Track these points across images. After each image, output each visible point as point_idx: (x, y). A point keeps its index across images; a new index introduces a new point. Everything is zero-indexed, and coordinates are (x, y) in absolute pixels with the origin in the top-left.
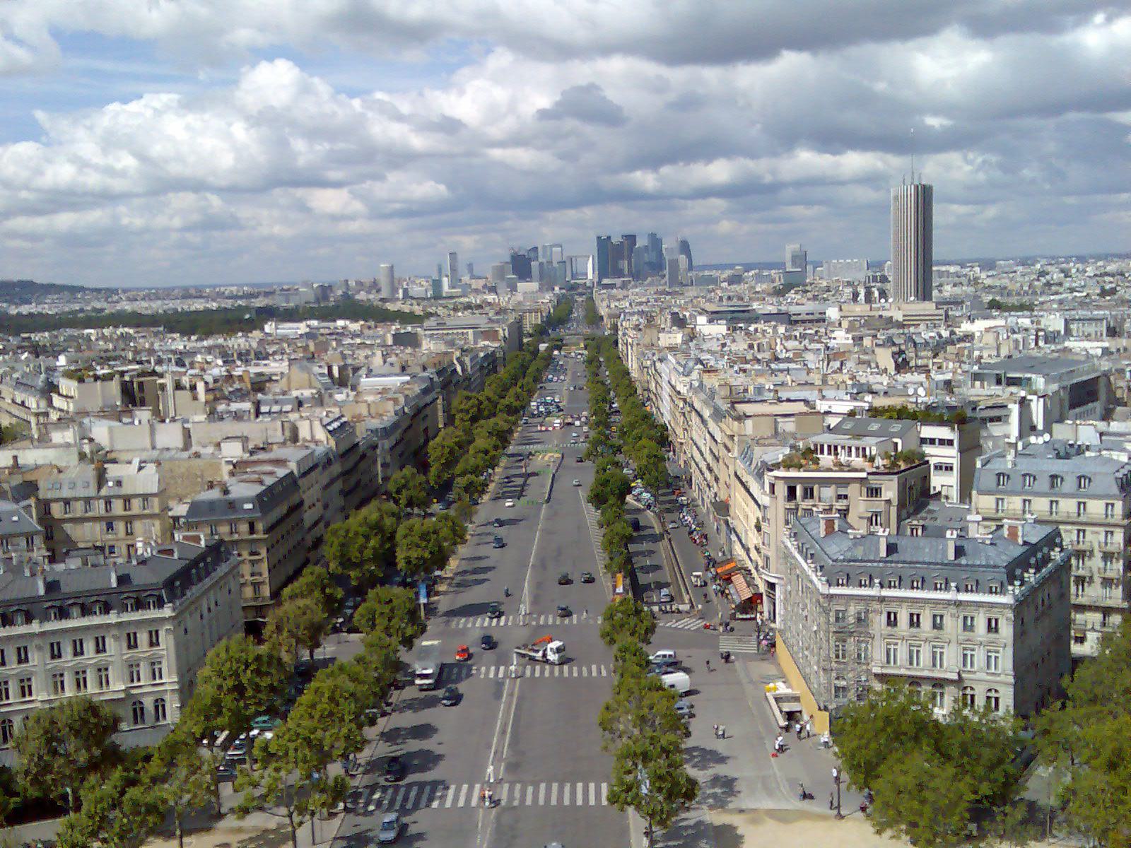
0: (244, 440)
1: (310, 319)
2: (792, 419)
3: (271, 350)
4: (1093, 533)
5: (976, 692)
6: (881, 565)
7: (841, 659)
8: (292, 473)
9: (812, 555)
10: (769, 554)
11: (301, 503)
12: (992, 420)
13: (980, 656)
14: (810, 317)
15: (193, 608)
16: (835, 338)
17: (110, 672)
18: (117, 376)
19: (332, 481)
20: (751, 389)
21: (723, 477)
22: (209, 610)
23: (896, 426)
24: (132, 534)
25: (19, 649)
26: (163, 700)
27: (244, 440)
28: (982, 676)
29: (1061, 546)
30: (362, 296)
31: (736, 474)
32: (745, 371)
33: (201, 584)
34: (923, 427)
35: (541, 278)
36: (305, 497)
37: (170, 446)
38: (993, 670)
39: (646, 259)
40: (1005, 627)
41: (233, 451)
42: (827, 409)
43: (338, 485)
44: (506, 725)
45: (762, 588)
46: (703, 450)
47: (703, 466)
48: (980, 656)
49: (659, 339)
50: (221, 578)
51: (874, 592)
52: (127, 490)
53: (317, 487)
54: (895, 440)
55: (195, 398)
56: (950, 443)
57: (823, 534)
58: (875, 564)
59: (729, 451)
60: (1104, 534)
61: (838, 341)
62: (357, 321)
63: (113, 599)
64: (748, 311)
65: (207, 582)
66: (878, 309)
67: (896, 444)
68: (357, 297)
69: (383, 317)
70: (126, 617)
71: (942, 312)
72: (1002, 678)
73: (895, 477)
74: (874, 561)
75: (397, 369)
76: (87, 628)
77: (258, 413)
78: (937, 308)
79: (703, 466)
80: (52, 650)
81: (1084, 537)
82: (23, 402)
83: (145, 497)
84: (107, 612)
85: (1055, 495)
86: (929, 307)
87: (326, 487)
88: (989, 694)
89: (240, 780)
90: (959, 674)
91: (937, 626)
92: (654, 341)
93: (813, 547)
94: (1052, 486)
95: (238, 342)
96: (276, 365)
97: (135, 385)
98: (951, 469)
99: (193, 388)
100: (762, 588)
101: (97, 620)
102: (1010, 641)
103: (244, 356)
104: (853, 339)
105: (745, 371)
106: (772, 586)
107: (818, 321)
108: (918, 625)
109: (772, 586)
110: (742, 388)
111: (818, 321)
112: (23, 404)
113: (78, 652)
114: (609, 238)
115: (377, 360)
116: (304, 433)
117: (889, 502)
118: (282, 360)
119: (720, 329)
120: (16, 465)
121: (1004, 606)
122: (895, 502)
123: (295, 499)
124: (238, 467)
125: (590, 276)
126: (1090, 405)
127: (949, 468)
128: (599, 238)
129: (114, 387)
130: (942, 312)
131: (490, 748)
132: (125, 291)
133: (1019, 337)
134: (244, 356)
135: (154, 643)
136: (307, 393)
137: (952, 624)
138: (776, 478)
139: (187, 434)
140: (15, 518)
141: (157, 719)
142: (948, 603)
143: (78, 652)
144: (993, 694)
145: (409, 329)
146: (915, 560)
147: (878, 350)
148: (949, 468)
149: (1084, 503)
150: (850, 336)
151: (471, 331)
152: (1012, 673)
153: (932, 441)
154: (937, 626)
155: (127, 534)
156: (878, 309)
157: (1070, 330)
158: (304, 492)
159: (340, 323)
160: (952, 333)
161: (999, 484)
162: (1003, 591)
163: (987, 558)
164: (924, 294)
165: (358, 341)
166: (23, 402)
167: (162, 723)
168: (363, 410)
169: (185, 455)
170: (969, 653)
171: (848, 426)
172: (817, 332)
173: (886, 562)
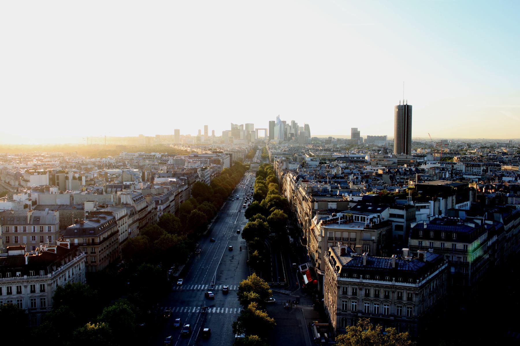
11: (118, 231)
15: (61, 275)
16: (366, 169)
19: (134, 222)
22: (69, 277)
29: (363, 330)
33: (65, 265)
36: (119, 229)
43: (137, 224)
50: (76, 263)
51: (394, 283)
53: (126, 225)
65: (69, 264)
82: (9, 182)
87: (130, 226)
89: (495, 183)
123: (115, 229)
126: (465, 203)
151: (208, 160)
158: (119, 227)
164: (408, 152)
166: (9, 182)
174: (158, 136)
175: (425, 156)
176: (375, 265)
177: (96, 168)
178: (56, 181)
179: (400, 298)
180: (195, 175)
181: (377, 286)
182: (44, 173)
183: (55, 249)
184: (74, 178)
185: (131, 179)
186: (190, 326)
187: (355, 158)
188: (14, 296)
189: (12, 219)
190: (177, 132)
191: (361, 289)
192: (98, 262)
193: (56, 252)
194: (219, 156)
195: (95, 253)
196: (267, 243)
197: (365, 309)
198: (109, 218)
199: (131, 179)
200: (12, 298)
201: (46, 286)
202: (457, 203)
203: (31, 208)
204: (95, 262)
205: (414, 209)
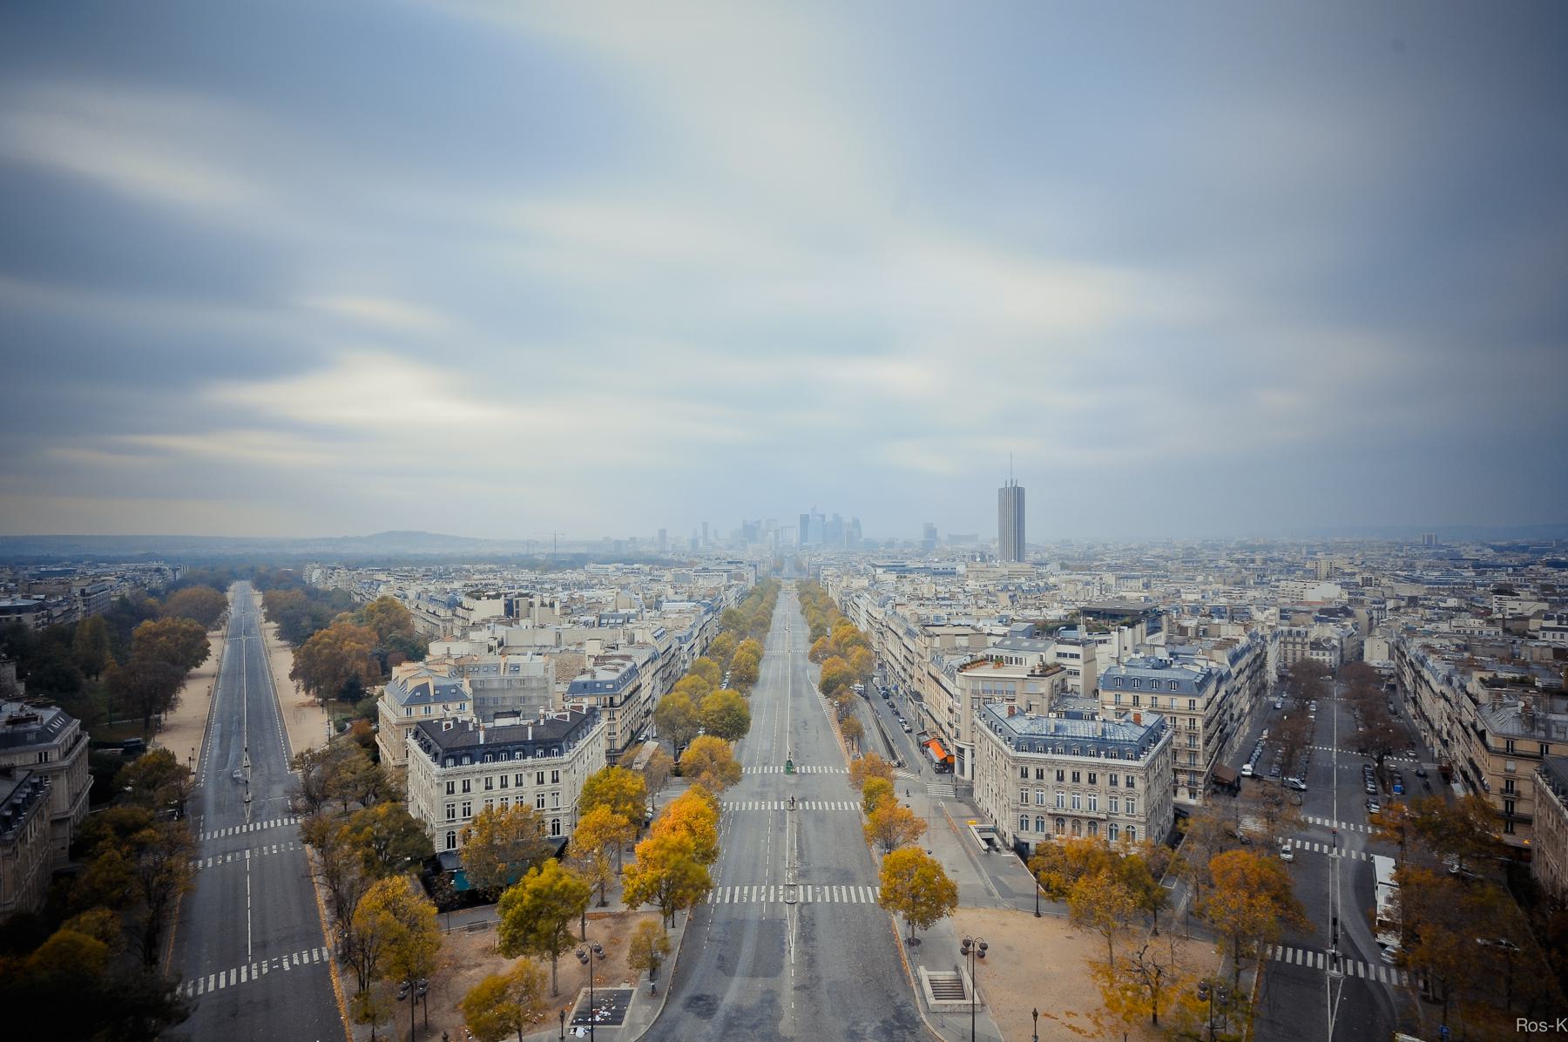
2: (967, 638)
3: (596, 581)
4: (1181, 719)
6: (1052, 738)
7: (1114, 800)
9: (1000, 730)
10: (960, 728)
12: (1100, 642)
13: (1122, 803)
18: (503, 596)
20: (932, 617)
21: (917, 674)
25: (464, 782)
26: (558, 820)
28: (1124, 817)
31: (929, 674)
32: (923, 605)
38: (1024, 803)
41: (594, 648)
43: (660, 674)
45: (954, 752)
46: (898, 657)
47: (898, 668)
48: (1122, 803)
53: (649, 675)
55: (553, 613)
56: (1077, 656)
57: (1007, 715)
58: (1047, 737)
59: (922, 658)
60: (1169, 719)
61: (970, 587)
64: (904, 566)
66: (992, 567)
69: (666, 564)
74: (1046, 735)
75: (685, 597)
77: (600, 625)
79: (898, 668)
84: (525, 758)
86: (1025, 567)
93: (1000, 724)
95: (571, 576)
97: (514, 603)
98: (1079, 674)
99: (552, 605)
100: (954, 752)
101: (519, 763)
103: (580, 586)
105: (923, 605)
106: (961, 751)
107: (951, 574)
108: (1078, 781)
109: (961, 751)
111: (951, 574)
112: (434, 613)
113: (504, 785)
115: (670, 592)
116: (638, 637)
119: (892, 577)
120: (449, 656)
121: (1138, 769)
124: (600, 660)
125: (795, 540)
126: (1158, 634)
129: (501, 602)
131: (785, 860)
132: (486, 540)
134: (580, 586)
135: (466, 790)
136: (633, 611)
137: (1050, 777)
140: (453, 691)
142: (1099, 766)
143: (504, 785)
144: (1024, 818)
147: (999, 594)
156: (992, 567)
162: (1137, 759)
164: (1019, 557)
165: (650, 578)
166: (435, 612)
168: (669, 624)
169: (557, 651)
170: (1025, 792)
171: (1008, 643)
173: (1055, 736)
174: (633, 540)
175: (1046, 564)
176: (1069, 731)
177: (560, 589)
178: (515, 610)
179: (1114, 783)
180: (720, 598)
181: (1076, 764)
182: (497, 596)
183: (568, 715)
184: (543, 605)
186: (1300, 839)
187: (941, 569)
188: (511, 792)
189: (476, 669)
190: (663, 533)
191: (478, 780)
192: (619, 734)
193: (568, 720)
194: (740, 568)
195: (614, 719)
196: (131, 742)
197: (1058, 802)
198: (629, 664)
200: (493, 796)
201: (561, 773)
202: (1148, 634)
203: (497, 651)
204: (615, 734)
205: (1093, 645)
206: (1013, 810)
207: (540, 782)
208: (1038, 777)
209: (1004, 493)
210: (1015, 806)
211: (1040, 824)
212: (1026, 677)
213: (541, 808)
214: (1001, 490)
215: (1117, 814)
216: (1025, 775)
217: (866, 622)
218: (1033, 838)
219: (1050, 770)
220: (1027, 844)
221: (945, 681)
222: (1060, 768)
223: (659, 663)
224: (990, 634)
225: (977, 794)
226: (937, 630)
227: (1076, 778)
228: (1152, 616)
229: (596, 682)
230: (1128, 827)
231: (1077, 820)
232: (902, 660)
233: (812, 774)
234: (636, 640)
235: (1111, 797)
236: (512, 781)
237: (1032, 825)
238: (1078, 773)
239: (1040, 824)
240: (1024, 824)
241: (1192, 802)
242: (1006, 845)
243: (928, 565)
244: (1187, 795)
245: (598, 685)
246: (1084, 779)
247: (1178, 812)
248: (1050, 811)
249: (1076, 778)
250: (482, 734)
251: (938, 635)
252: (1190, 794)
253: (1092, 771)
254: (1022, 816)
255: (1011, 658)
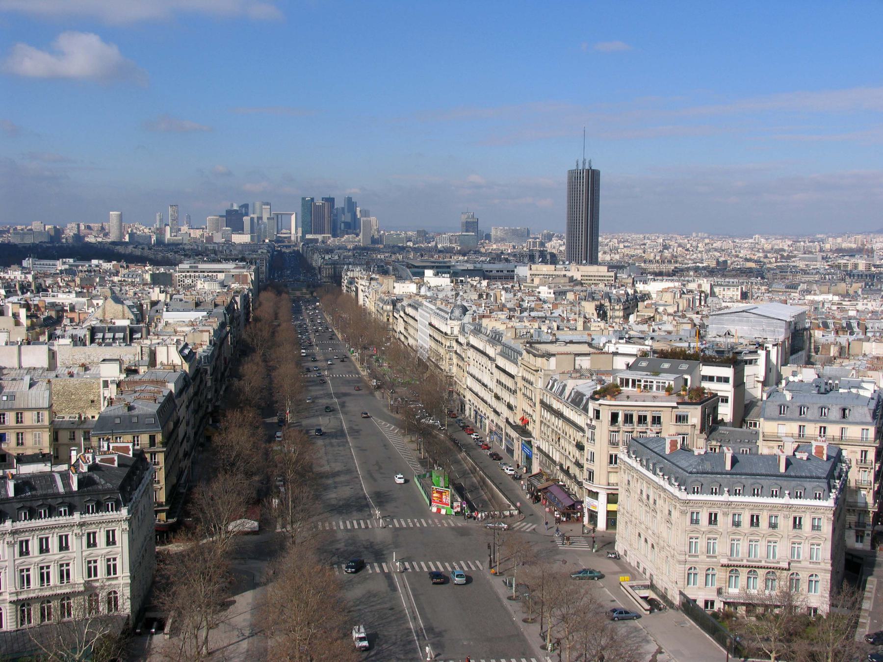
0: (120, 361)
1: (66, 258)
3: (49, 282)
5: (800, 576)
8: (171, 392)
14: (500, 274)
17: (71, 567)
23: (684, 366)
24: (22, 444)
26: (115, 592)
27: (120, 361)
30: (91, 239)
34: (704, 367)
35: (252, 231)
37: (37, 366)
39: (343, 219)
40: (826, 524)
42: (615, 350)
44: (413, 612)
49: (394, 288)
52: (19, 403)
54: (686, 376)
56: (726, 380)
60: (860, 453)
62: (110, 261)
63: (76, 500)
67: (686, 380)
68: (87, 239)
70: (88, 517)
71: (612, 274)
72: (822, 565)
73: (699, 407)
76: (53, 528)
77: (92, 340)
78: (608, 271)
80: (108, 537)
81: (824, 433)
83: (38, 410)
85: (824, 421)
88: (811, 578)
90: (789, 564)
91: (773, 526)
92: (391, 288)
94: (844, 416)
96: (65, 296)
98: (727, 401)
101: (62, 520)
102: (829, 535)
104: (554, 293)
108: (758, 525)
110: (525, 331)
113: (44, 549)
114: (312, 199)
116: (161, 357)
117: (694, 426)
118: (69, 292)
122: (698, 427)
127: (725, 400)
128: (304, 199)
130: (612, 274)
133: (690, 296)
137: (785, 524)
138: (600, 405)
139: (52, 355)
141: (63, 615)
143: (44, 549)
144: (813, 578)
145: (162, 270)
146: (754, 472)
148: (725, 400)
149: (825, 428)
150: (552, 291)
152: (830, 561)
153: (711, 379)
154: (773, 526)
155: (18, 444)
157: (714, 293)
159: (95, 262)
160: (635, 292)
161: (781, 414)
163: (810, 471)
167: (66, 619)
172: (513, 287)
181: (756, 505)
185: (124, 314)
199: (124, 314)
206: (679, 562)
207: (92, 544)
208: (710, 523)
209: (574, 177)
210: (682, 558)
211: (709, 574)
212: (675, 404)
213: (112, 576)
214: (571, 172)
215: (800, 562)
216: (695, 522)
217: (428, 339)
218: (700, 594)
219: (725, 514)
220: (695, 601)
221: (568, 413)
222: (797, 515)
223: (191, 390)
224: (615, 354)
225: (619, 548)
226: (552, 348)
227: (755, 521)
228: (59, 308)
229: (131, 417)
230: (812, 575)
231: (752, 570)
232: (492, 384)
233: (408, 527)
234: (158, 362)
235: (794, 543)
236: (54, 544)
237: (701, 579)
238: (800, 519)
239: (709, 574)
240: (690, 575)
241: (859, 546)
242: (671, 605)
243: (478, 266)
244: (854, 538)
245: (135, 420)
246: (764, 523)
247: (850, 557)
248: (725, 561)
249: (755, 521)
250: (11, 485)
251: (554, 355)
252: (857, 537)
253: (713, 511)
254: (690, 569)
255: (627, 380)
